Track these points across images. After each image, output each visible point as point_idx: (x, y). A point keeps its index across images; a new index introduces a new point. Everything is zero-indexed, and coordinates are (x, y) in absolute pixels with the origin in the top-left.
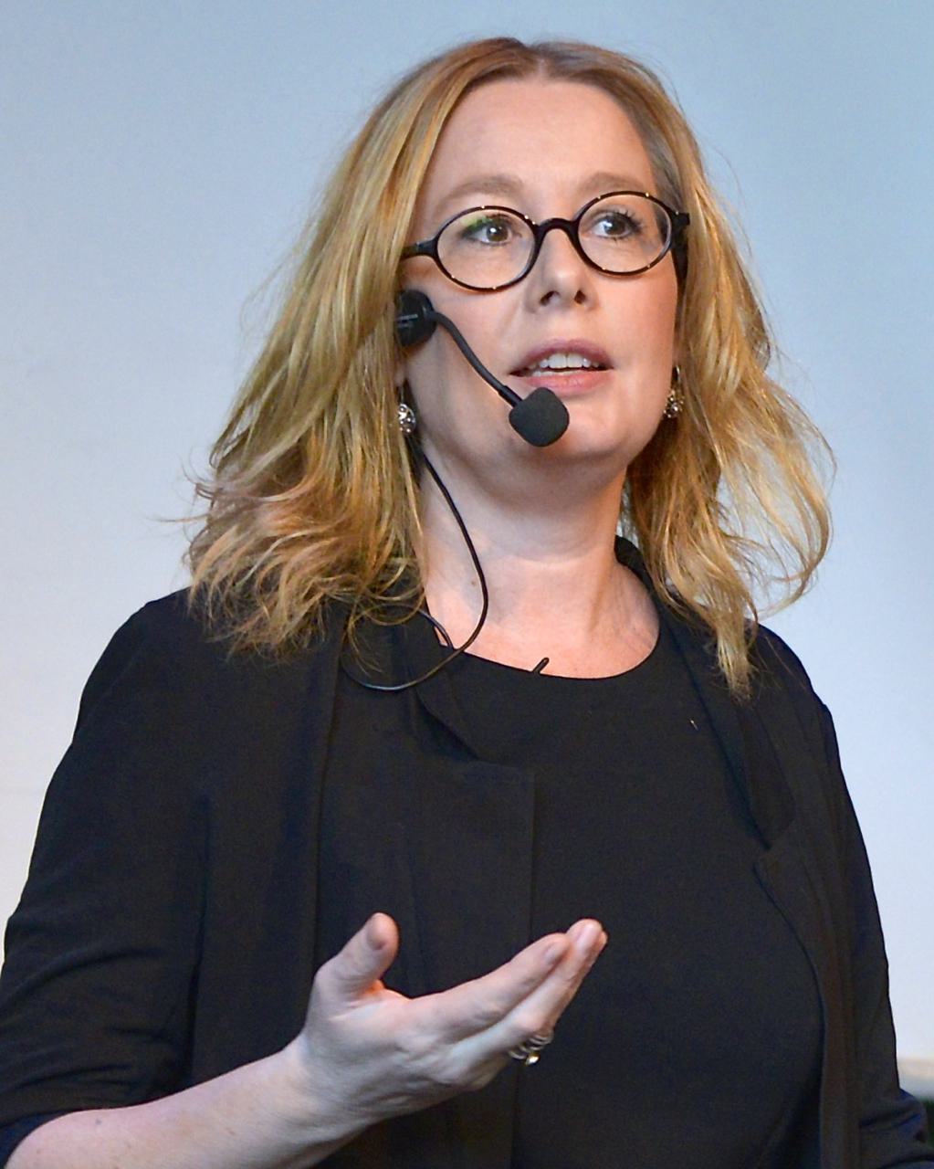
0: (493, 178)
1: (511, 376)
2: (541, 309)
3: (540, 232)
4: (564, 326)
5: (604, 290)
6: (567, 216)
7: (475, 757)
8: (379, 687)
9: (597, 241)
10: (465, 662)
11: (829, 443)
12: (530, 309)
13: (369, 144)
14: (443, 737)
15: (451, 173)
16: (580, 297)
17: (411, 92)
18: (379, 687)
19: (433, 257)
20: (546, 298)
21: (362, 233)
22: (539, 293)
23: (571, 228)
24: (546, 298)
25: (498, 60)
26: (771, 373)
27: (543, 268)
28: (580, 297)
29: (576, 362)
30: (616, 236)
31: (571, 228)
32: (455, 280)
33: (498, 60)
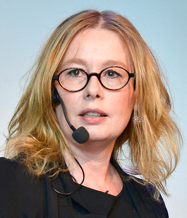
0: (79, 60)
1: (79, 116)
2: (87, 98)
3: (89, 76)
4: (93, 105)
5: (106, 93)
6: (98, 72)
7: (90, 213)
8: (56, 191)
9: (105, 79)
10: (81, 187)
11: (82, 182)
12: (84, 98)
13: (61, 34)
14: (77, 206)
15: (70, 56)
16: (98, 96)
17: (71, 21)
18: (56, 191)
19: (57, 80)
20: (88, 96)
21: (44, 68)
22: (86, 94)
23: (98, 76)
24: (88, 96)
25: (91, 19)
26: (171, 114)
27: (87, 88)
28: (98, 96)
29: (96, 114)
30: (112, 77)
31: (98, 76)
32: (64, 88)
33: (91, 19)
